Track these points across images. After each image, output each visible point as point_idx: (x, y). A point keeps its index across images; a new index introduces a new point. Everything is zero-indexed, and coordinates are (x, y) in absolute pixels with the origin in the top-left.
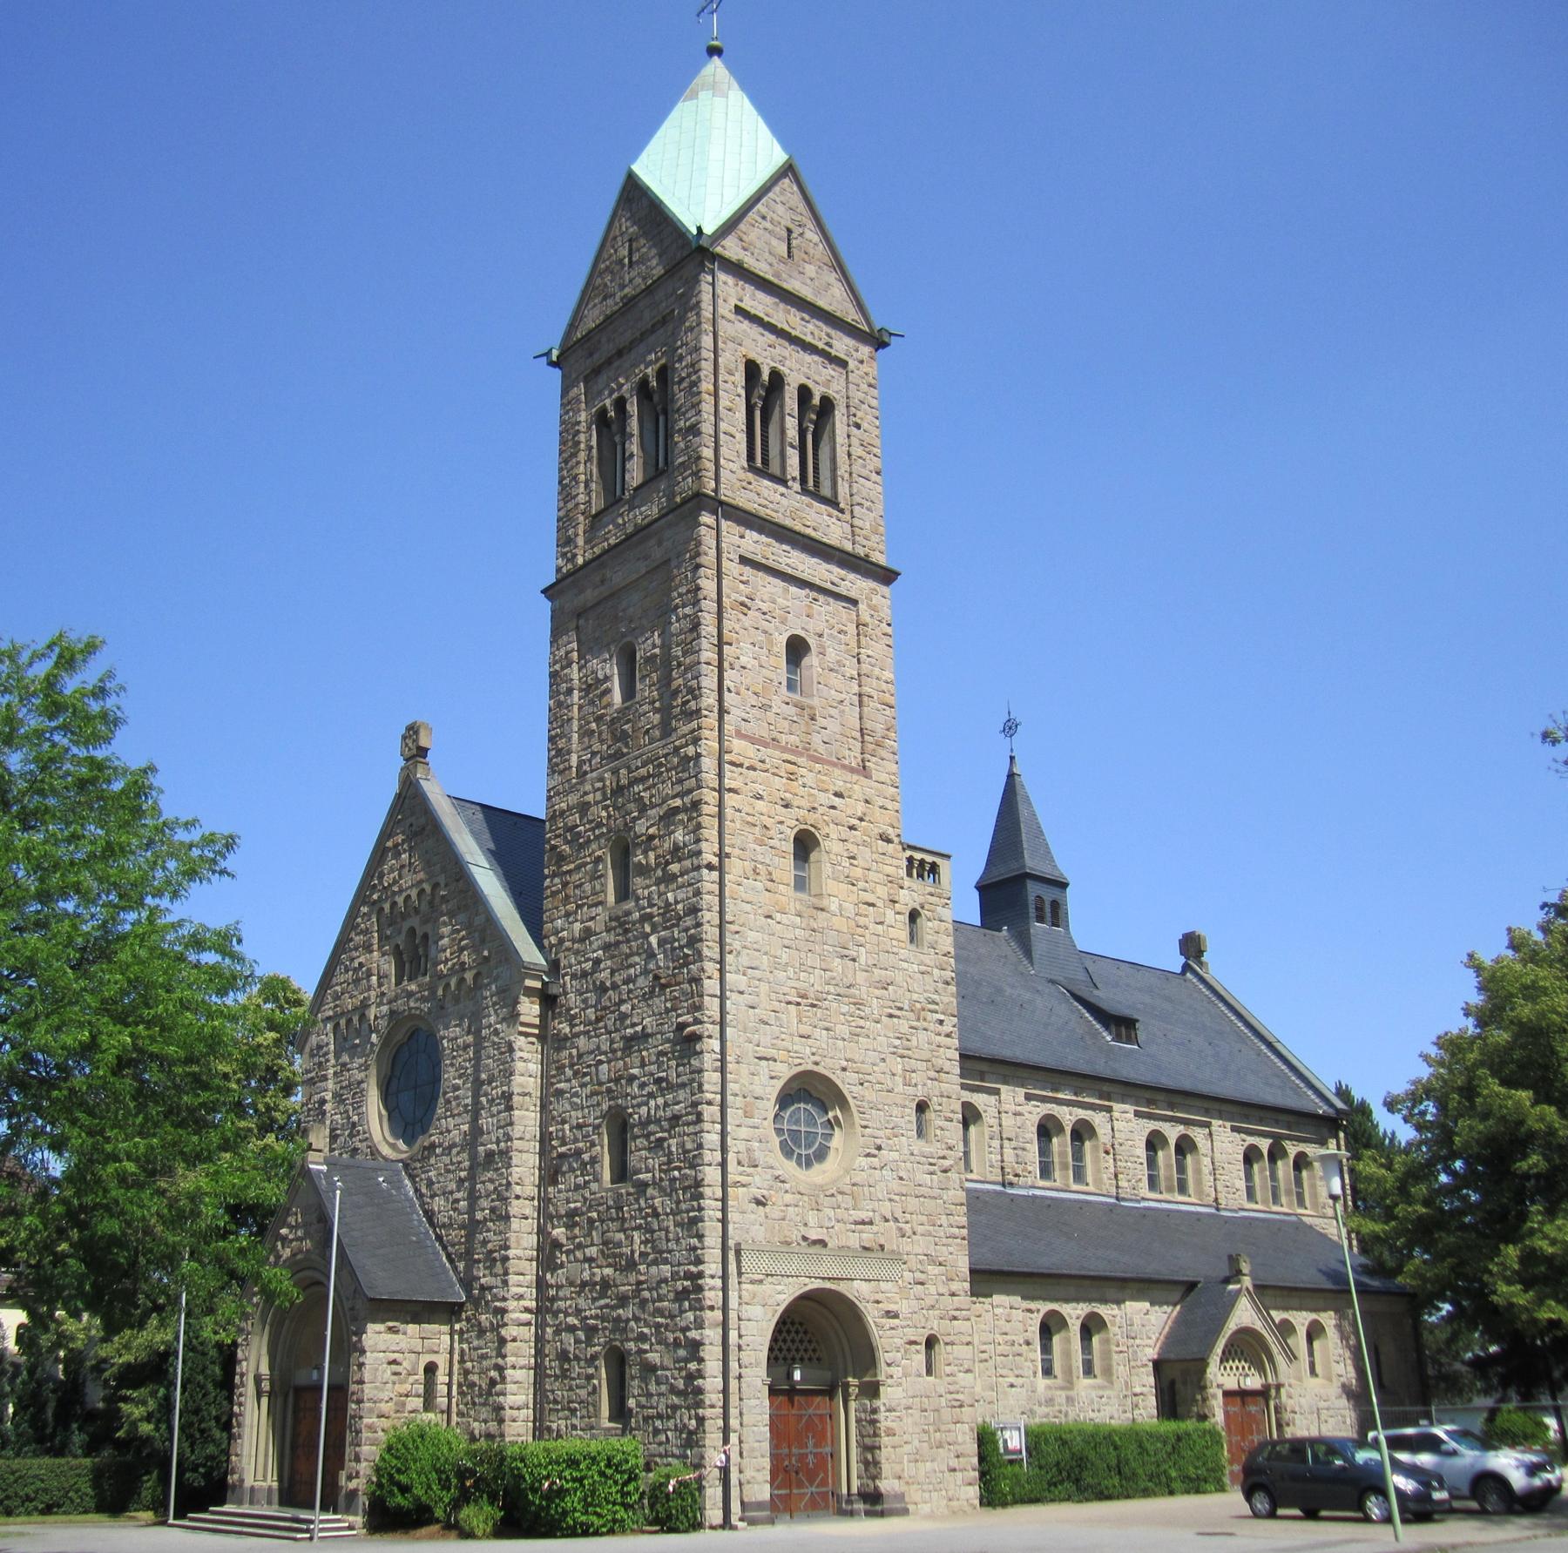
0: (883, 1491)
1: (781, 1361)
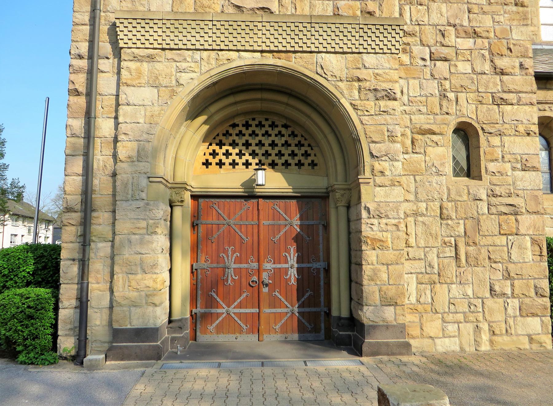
0: (365, 321)
1: (241, 167)
